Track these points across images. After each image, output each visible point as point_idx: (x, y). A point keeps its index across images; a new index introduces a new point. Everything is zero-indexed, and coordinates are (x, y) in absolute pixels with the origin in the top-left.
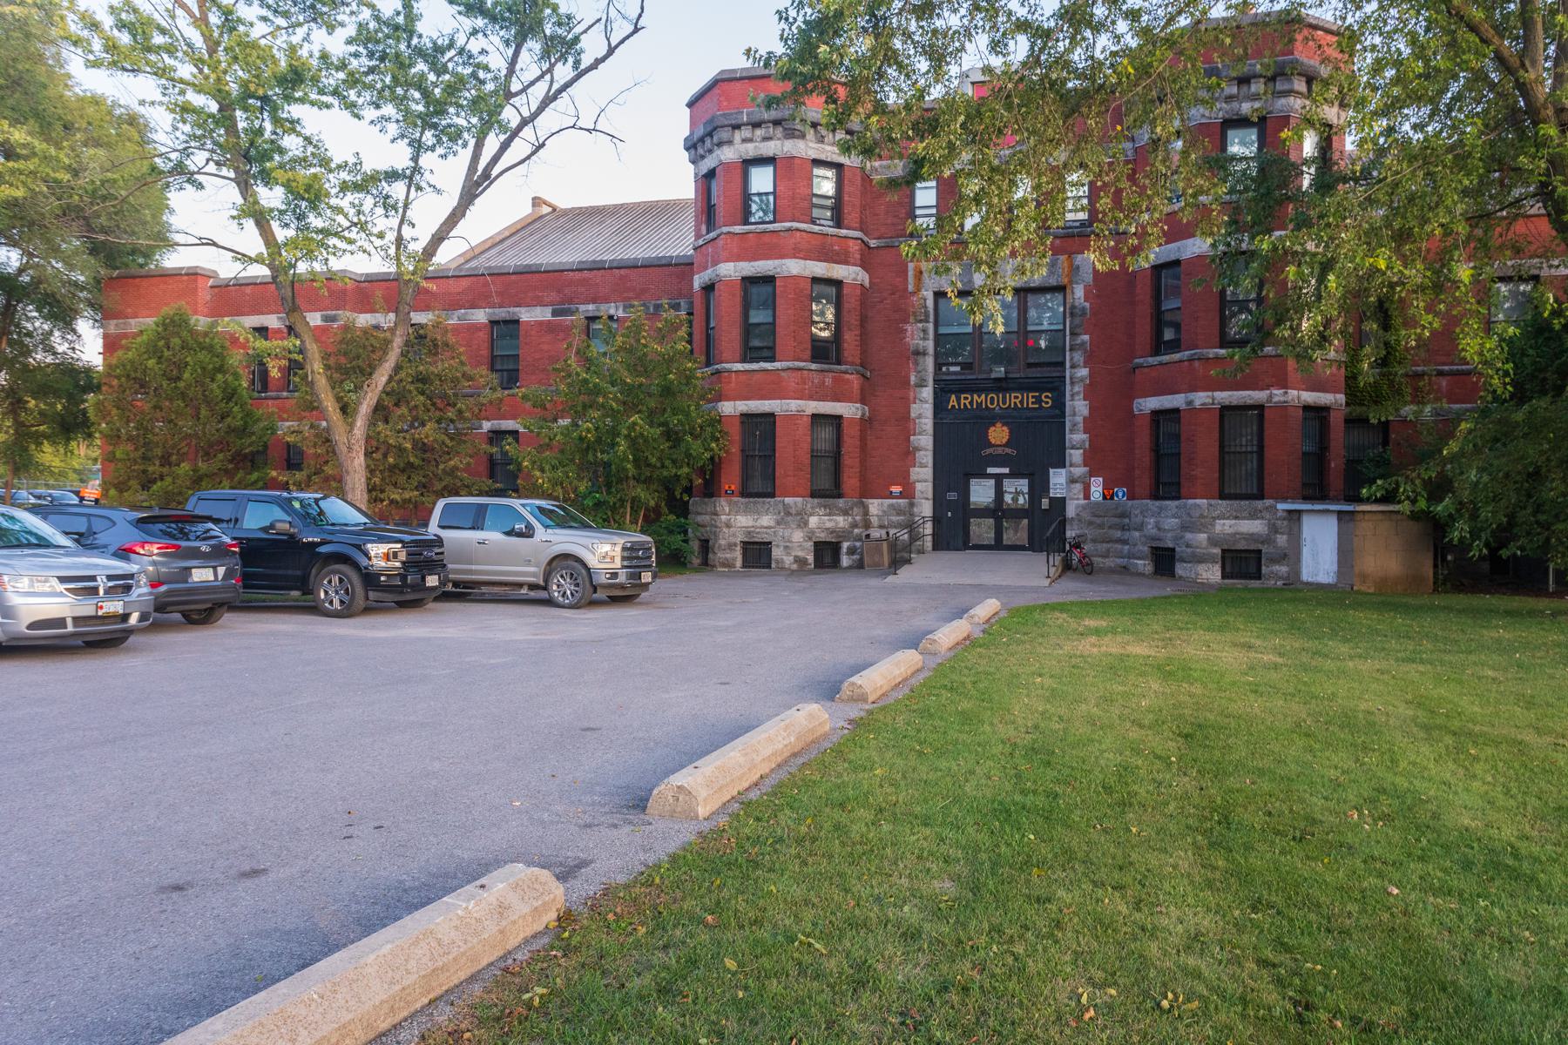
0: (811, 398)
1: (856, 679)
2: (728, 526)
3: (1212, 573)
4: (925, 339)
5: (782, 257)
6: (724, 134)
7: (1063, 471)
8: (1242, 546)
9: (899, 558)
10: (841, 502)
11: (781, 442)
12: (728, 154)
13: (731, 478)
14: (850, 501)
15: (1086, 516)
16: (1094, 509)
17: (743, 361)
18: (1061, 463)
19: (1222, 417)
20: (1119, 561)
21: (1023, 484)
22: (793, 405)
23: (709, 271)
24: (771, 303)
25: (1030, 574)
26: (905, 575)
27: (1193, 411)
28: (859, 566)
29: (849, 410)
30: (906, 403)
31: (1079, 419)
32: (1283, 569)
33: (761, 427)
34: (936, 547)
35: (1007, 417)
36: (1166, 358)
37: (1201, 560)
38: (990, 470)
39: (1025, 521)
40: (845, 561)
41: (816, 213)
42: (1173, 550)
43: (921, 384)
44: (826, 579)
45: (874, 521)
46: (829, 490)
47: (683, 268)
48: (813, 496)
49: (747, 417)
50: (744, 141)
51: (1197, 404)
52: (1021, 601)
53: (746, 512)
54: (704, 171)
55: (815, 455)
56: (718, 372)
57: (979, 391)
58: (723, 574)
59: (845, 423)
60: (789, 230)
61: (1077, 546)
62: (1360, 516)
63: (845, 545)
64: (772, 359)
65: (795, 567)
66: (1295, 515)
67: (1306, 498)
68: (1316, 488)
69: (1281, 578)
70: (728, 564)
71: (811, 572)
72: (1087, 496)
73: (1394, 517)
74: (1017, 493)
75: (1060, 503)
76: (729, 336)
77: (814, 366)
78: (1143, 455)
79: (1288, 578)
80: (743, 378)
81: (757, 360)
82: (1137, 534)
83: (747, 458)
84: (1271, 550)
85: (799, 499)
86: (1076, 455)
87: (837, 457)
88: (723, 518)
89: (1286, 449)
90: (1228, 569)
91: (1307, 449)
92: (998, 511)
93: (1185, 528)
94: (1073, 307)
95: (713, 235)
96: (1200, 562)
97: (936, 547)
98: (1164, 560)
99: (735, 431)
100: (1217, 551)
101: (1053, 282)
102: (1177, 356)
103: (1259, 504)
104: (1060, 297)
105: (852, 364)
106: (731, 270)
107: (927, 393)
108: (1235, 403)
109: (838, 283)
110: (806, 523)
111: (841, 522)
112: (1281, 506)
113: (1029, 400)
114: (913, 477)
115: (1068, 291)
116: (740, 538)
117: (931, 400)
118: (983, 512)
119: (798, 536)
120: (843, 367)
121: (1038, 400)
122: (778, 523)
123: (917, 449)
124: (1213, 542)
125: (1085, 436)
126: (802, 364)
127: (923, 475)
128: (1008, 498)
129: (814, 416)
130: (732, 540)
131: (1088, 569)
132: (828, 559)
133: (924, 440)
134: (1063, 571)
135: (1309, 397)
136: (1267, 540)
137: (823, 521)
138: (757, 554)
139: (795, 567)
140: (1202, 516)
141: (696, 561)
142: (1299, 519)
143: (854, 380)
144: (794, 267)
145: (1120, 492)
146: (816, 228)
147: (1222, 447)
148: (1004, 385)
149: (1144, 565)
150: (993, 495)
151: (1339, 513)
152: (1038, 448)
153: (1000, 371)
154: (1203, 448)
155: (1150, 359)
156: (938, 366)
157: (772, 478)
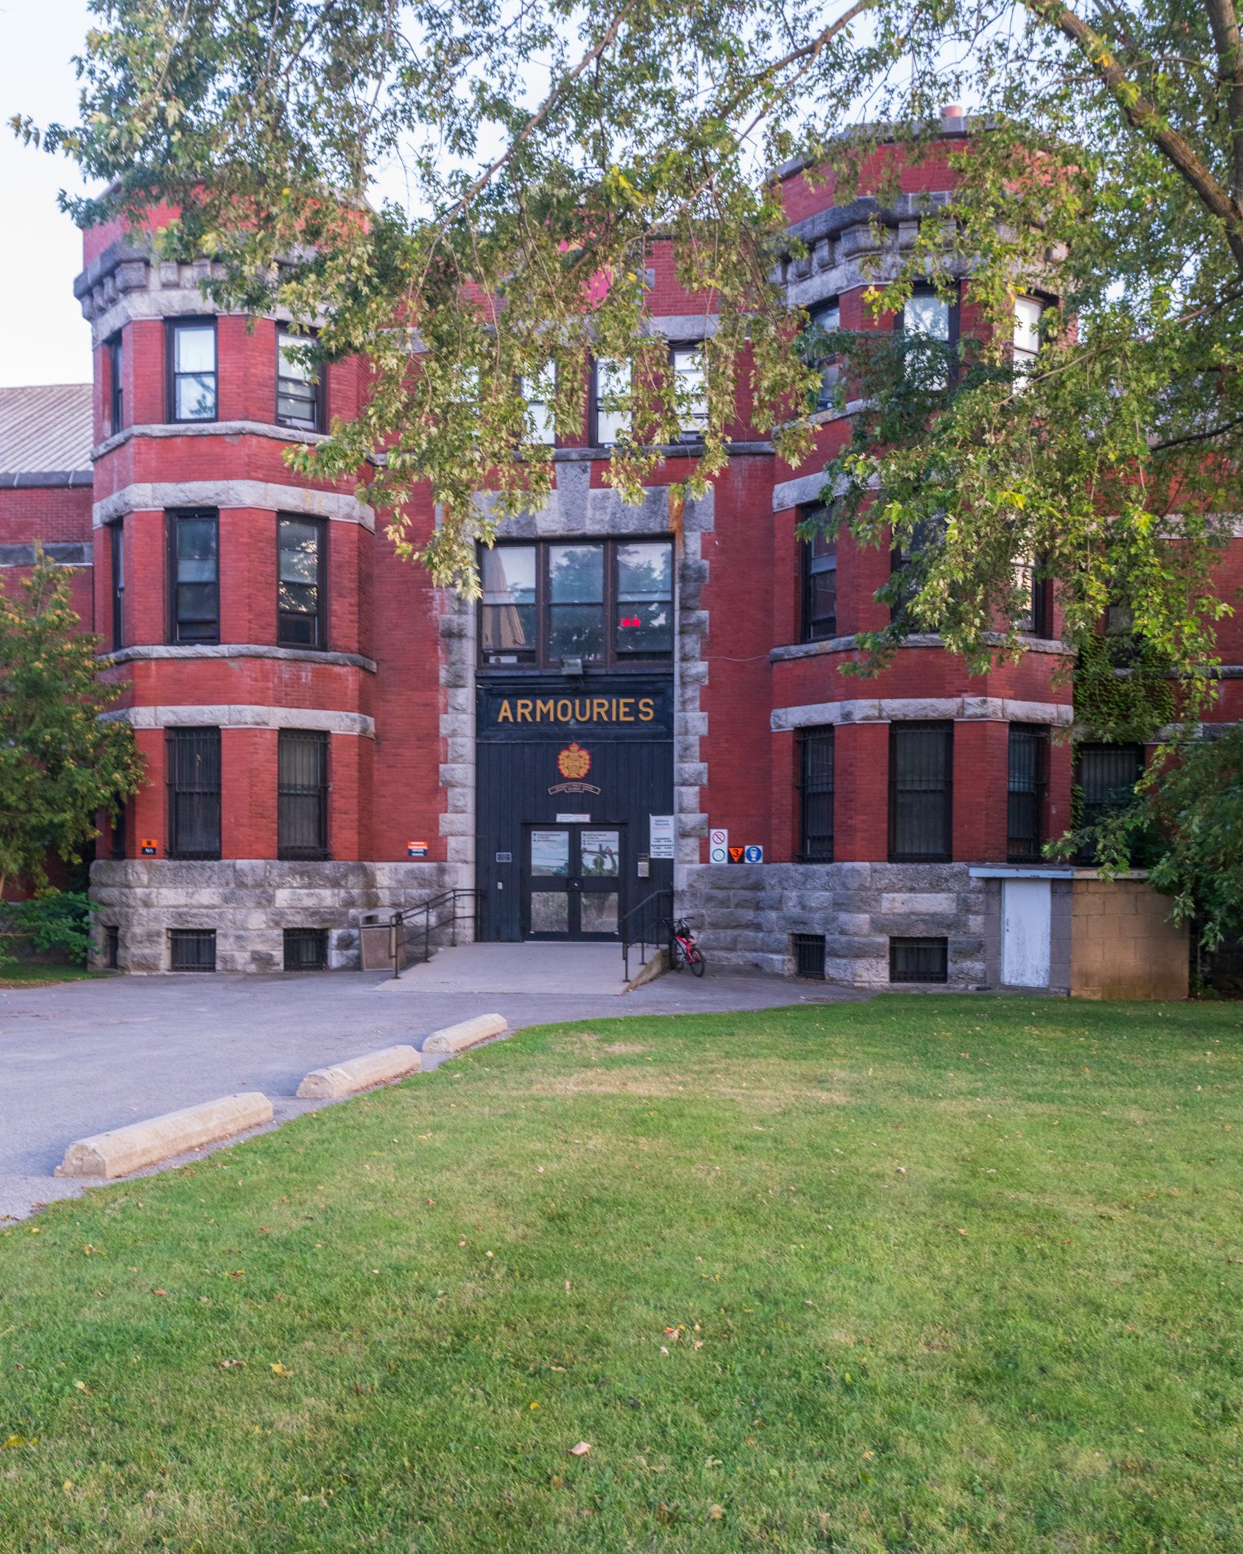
0: (278, 702)
1: (91, 1143)
2: (147, 904)
3: (875, 974)
4: (461, 612)
5: (228, 476)
6: (132, 274)
7: (670, 819)
8: (919, 931)
9: (415, 949)
10: (328, 867)
11: (230, 772)
12: (140, 307)
13: (151, 827)
14: (342, 865)
15: (703, 888)
16: (717, 878)
17: (170, 641)
18: (667, 809)
19: (892, 737)
20: (751, 956)
21: (610, 840)
22: (248, 714)
23: (115, 497)
24: (210, 551)
25: (596, 976)
26: (416, 979)
27: (851, 727)
28: (356, 966)
29: (341, 723)
30: (432, 712)
31: (694, 740)
32: (976, 966)
33: (194, 745)
34: (480, 936)
35: (588, 736)
36: (814, 647)
37: (860, 953)
38: (561, 818)
39: (614, 897)
40: (335, 958)
41: (285, 407)
42: (822, 938)
43: (456, 683)
44: (309, 987)
45: (385, 896)
46: (307, 849)
47: (78, 491)
48: (282, 856)
49: (176, 733)
50: (166, 286)
51: (857, 717)
52: (533, 1017)
53: (176, 881)
54: (105, 333)
55: (285, 792)
56: (129, 660)
57: (545, 695)
58: (139, 982)
59: (334, 744)
60: (239, 433)
61: (685, 934)
62: (1081, 887)
63: (335, 934)
64: (214, 640)
65: (252, 968)
66: (994, 886)
67: (1013, 861)
68: (1025, 849)
69: (974, 979)
70: (147, 965)
71: (277, 976)
72: (705, 858)
73: (1132, 888)
74: (603, 853)
75: (664, 869)
76: (146, 602)
77: (282, 652)
78: (784, 796)
79: (983, 980)
80: (168, 669)
81: (191, 641)
82: (773, 915)
83: (176, 798)
84: (961, 938)
85: (260, 862)
86: (688, 796)
87: (322, 795)
88: (139, 891)
89: (982, 788)
90: (901, 967)
91: (1016, 786)
92: (573, 881)
93: (838, 905)
94: (685, 567)
95: (119, 438)
96: (858, 956)
97: (480, 936)
98: (810, 953)
99: (157, 755)
100: (884, 940)
101: (655, 527)
102: (829, 645)
103: (944, 869)
104: (667, 547)
105: (346, 649)
106: (148, 496)
107: (465, 697)
108: (911, 716)
109: (320, 522)
110: (271, 900)
111: (328, 898)
112: (976, 872)
113: (619, 709)
114: (444, 828)
115: (678, 541)
116: (166, 923)
117: (471, 708)
118: (551, 883)
119: (257, 920)
120: (330, 655)
121: (634, 710)
122: (226, 900)
123: (451, 785)
124: (878, 926)
125: (703, 766)
126: (262, 649)
127: (459, 825)
128: (588, 861)
129: (284, 732)
130: (154, 926)
131: (698, 968)
132: (308, 955)
133: (461, 772)
134: (663, 972)
135: (1019, 709)
136: (956, 923)
137: (298, 896)
138: (194, 949)
139: (252, 968)
140: (862, 888)
141: (101, 960)
142: (1000, 892)
143: (349, 677)
144: (247, 493)
145: (753, 852)
146: (284, 432)
147: (892, 783)
148: (582, 685)
149: (783, 962)
150: (565, 856)
151: (1054, 881)
152: (632, 784)
153: (574, 665)
154: (865, 784)
155: (793, 649)
156: (482, 656)
157: (214, 824)
